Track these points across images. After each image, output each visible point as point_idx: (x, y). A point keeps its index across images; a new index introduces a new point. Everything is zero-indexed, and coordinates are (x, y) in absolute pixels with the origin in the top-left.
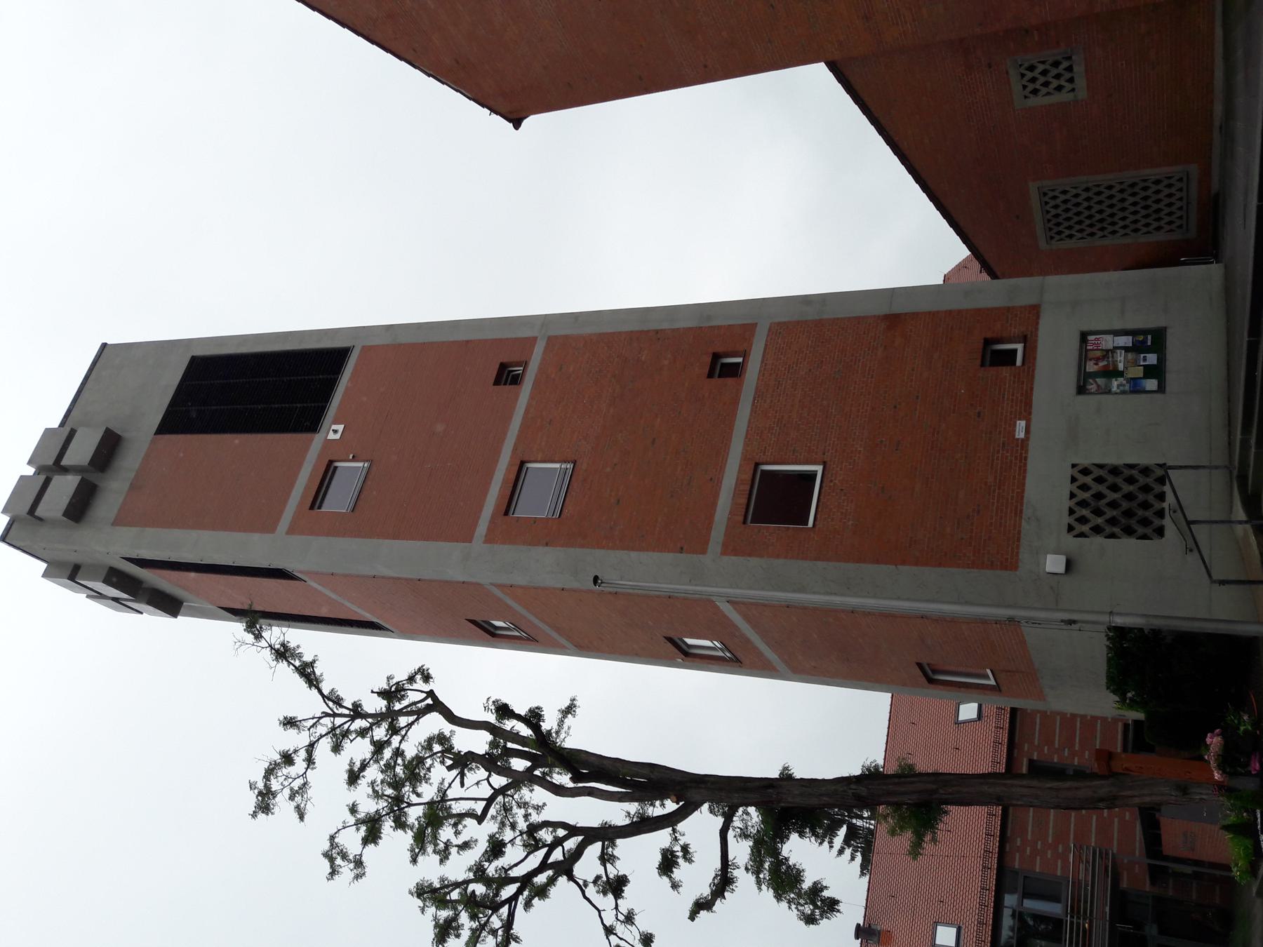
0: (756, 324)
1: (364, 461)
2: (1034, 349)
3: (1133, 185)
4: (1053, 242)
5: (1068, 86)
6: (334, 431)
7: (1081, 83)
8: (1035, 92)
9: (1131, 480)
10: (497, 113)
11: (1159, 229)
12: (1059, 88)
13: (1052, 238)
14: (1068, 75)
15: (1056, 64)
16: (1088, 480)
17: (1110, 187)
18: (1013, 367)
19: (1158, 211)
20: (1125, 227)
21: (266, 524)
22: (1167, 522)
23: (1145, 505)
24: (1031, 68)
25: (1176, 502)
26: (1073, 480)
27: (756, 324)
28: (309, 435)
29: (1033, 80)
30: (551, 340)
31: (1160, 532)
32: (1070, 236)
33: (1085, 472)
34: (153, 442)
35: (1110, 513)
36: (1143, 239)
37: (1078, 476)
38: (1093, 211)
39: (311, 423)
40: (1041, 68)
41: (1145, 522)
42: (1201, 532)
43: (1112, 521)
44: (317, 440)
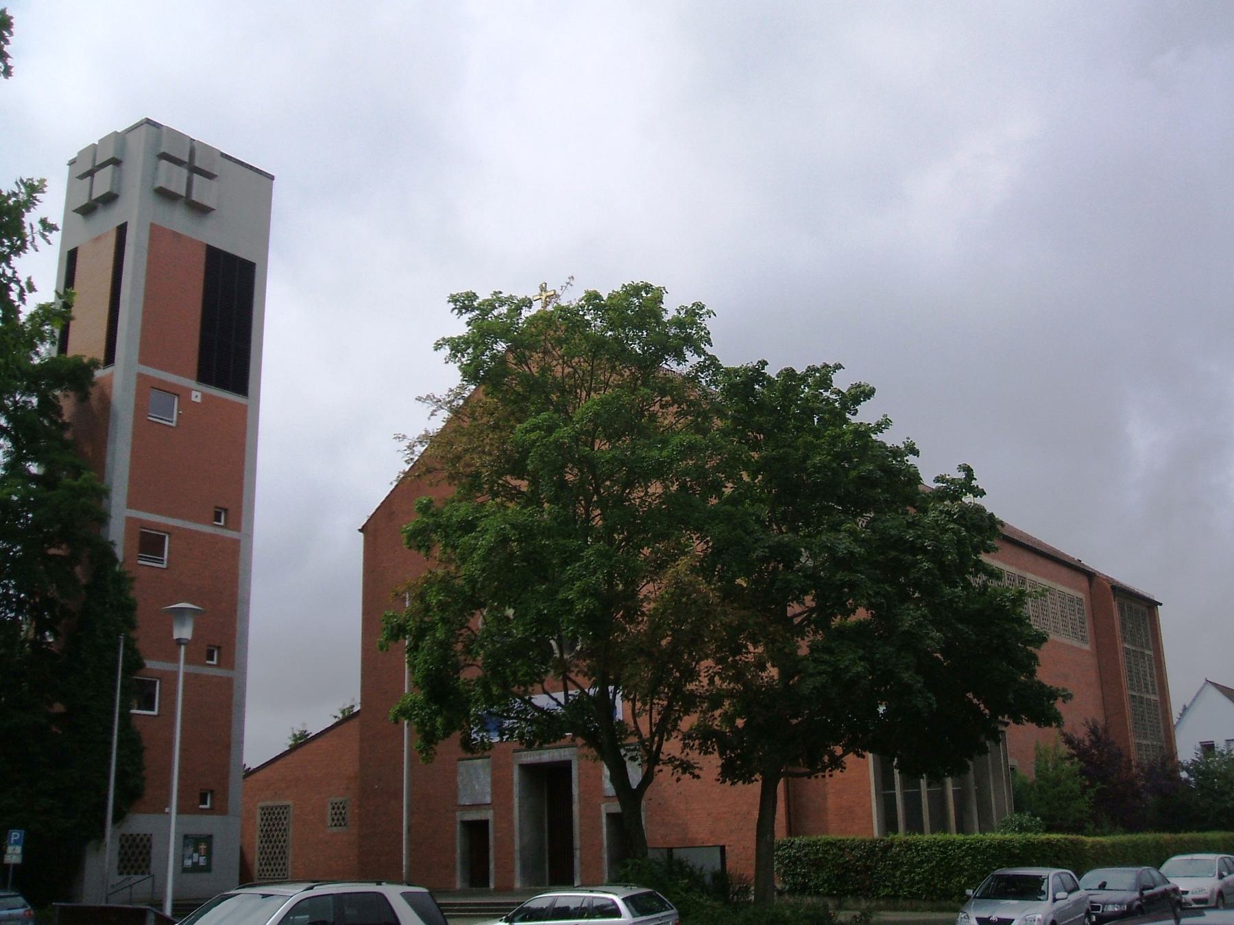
0: (126, 222)
1: (178, 422)
2: (207, 814)
3: (284, 853)
4: (260, 810)
5: (333, 824)
6: (198, 394)
7: (335, 829)
8: (333, 808)
9: (144, 860)
10: (368, 521)
11: (261, 865)
12: (333, 820)
13: (263, 809)
14: (338, 824)
15: (343, 819)
16: (145, 841)
17: (284, 864)
18: (198, 801)
19: (270, 864)
20: (264, 848)
21: (146, 357)
22: (125, 876)
23: (140, 867)
24: (344, 808)
25: (696, 845)
26: (145, 835)
27: (126, 222)
28: (195, 375)
29: (338, 808)
30: (236, 542)
31: (121, 874)
32: (262, 820)
33: (149, 840)
34: (199, 243)
35: (130, 852)
36: (257, 856)
37: (147, 837)
38: (274, 832)
39: (204, 376)
40: (343, 812)
41: (125, 867)
42: (128, 889)
43: (126, 854)
44: (190, 383)
